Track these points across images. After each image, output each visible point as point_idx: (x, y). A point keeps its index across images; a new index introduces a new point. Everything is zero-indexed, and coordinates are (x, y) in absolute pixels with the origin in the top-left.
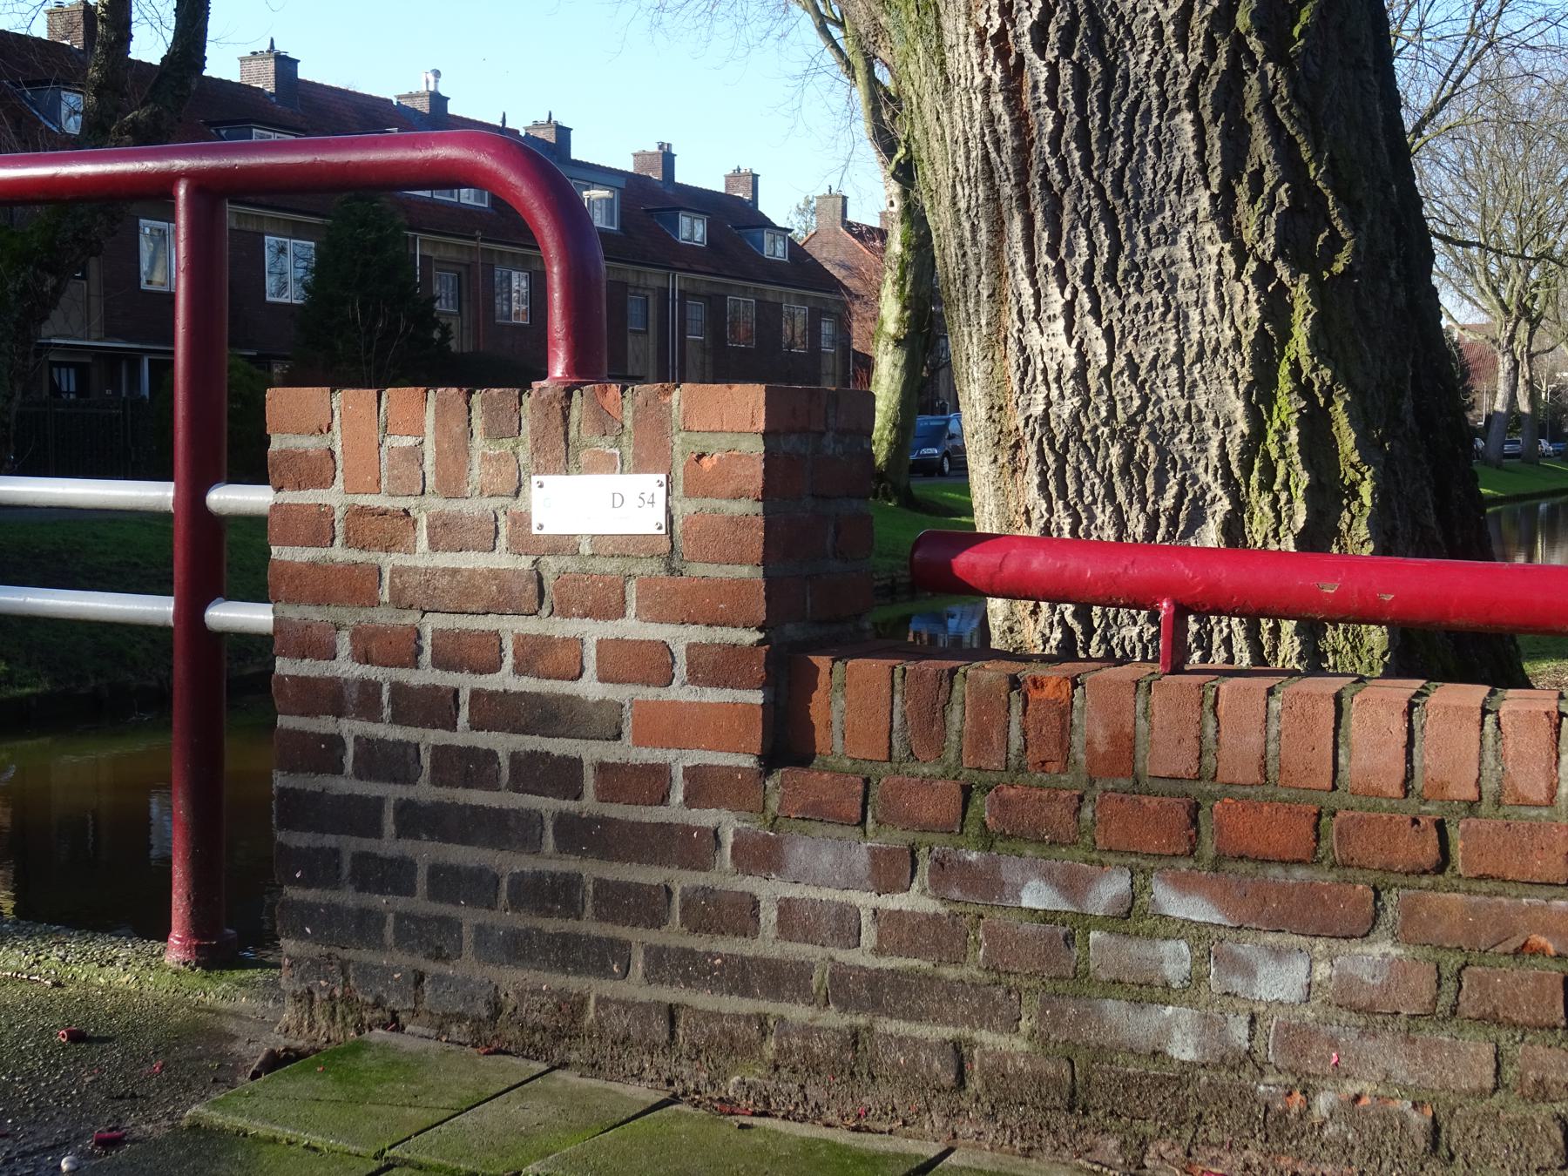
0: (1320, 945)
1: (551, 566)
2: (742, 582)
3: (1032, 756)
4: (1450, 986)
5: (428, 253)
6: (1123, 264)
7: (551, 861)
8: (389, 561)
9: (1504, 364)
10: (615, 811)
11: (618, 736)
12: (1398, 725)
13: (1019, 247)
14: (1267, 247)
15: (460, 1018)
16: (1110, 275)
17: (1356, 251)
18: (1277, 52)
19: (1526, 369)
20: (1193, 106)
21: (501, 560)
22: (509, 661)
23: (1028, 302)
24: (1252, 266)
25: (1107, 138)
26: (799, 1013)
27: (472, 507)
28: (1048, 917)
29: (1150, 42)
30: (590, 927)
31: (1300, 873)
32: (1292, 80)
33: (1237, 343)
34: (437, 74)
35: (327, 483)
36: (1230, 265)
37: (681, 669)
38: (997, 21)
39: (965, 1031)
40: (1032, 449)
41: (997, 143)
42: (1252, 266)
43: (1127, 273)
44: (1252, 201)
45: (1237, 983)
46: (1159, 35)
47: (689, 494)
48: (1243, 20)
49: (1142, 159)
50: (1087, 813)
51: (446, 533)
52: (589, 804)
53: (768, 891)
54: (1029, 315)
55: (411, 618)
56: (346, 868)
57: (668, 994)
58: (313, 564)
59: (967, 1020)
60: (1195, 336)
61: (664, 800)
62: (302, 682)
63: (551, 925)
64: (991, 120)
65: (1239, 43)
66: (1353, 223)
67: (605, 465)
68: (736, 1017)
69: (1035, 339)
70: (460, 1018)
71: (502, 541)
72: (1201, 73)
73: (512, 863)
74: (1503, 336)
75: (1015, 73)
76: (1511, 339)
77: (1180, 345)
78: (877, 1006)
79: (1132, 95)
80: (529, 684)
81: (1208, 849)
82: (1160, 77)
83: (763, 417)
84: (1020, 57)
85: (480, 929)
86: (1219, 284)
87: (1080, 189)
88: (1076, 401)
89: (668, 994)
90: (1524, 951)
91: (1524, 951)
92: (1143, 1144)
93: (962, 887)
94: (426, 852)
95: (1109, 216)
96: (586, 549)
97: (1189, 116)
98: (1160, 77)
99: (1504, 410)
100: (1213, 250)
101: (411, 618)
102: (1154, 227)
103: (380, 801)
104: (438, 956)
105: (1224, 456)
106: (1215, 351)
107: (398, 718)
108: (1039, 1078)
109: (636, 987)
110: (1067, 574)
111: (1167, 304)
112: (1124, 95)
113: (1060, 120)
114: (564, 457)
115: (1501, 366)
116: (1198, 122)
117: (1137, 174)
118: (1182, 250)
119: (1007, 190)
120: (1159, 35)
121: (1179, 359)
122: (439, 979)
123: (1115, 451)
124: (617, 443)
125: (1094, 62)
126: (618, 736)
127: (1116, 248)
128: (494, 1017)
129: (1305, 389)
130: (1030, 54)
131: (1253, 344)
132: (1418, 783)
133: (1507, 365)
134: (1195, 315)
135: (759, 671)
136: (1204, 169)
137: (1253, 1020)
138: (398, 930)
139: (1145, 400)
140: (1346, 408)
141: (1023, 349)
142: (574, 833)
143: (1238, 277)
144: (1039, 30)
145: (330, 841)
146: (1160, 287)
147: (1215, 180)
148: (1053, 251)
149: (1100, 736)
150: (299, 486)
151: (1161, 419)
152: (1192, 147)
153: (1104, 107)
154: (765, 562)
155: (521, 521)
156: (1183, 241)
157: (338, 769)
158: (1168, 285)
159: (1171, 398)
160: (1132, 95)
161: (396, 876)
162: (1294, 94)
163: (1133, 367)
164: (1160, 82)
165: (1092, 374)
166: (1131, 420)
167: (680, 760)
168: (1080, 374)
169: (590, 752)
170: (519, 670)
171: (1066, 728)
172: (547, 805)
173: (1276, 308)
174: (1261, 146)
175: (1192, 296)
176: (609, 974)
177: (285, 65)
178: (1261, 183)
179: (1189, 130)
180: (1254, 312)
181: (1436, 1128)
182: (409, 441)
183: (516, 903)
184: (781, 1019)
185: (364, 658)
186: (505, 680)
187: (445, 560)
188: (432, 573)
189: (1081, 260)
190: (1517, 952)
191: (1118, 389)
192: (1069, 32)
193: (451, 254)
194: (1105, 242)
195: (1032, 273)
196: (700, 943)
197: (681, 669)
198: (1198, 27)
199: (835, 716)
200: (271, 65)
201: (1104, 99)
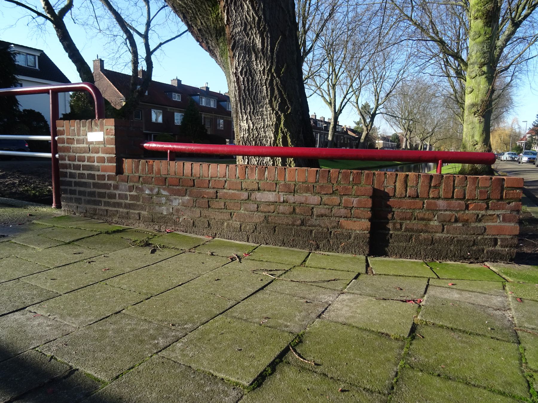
0: (180, 197)
1: (91, 146)
2: (112, 148)
3: (149, 172)
4: (195, 203)
5: (205, 116)
6: (255, 111)
7: (93, 189)
8: (72, 146)
9: (405, 140)
10: (99, 182)
11: (99, 171)
12: (190, 166)
13: (239, 109)
14: (277, 109)
15: (82, 212)
16: (253, 113)
17: (291, 110)
18: (278, 76)
20: (266, 85)
21: (85, 145)
22: (86, 160)
23: (241, 118)
24: (275, 112)
25: (252, 90)
26: (121, 210)
27: (81, 137)
28: (149, 195)
29: (259, 74)
30: (97, 199)
31: (178, 187)
32: (281, 81)
33: (272, 125)
34: (207, 83)
35: (64, 134)
36: (271, 112)
37: (106, 161)
38: (235, 70)
39: (140, 211)
40: (241, 142)
41: (236, 91)
42: (275, 112)
43: (256, 113)
44: (275, 101)
45: (171, 203)
46: (260, 73)
47: (106, 135)
48: (273, 71)
49: (258, 94)
50: (153, 180)
51: (79, 141)
52: (96, 181)
53: (117, 192)
54: (241, 120)
55: (75, 154)
56: (68, 192)
57: (106, 208)
58: (63, 147)
59: (140, 210)
60: (266, 124)
61: (105, 180)
62: (62, 164)
63: (93, 199)
64: (235, 87)
65: (272, 75)
66: (291, 106)
67: (96, 131)
68: (114, 211)
69: (242, 124)
70: (82, 212)
71: (85, 143)
72: (267, 80)
73: (88, 190)
74: (405, 134)
75: (238, 79)
76: (406, 135)
77: (264, 125)
78: (130, 208)
79: (256, 83)
80: (89, 163)
81: (167, 184)
82: (261, 80)
84: (239, 77)
85: (84, 200)
86: (270, 115)
87: (248, 99)
88: (248, 134)
89: (106, 208)
90: (203, 197)
91: (203, 197)
92: (161, 226)
93: (139, 191)
94: (78, 189)
95: (253, 103)
96: (95, 143)
97: (265, 87)
98: (261, 80)
100: (269, 109)
101: (75, 154)
102: (260, 105)
103: (72, 181)
104: (80, 204)
105: (270, 143)
106: (269, 126)
107: (74, 169)
108: (148, 218)
109: (103, 207)
111: (262, 118)
112: (255, 83)
113: (245, 87)
114: (91, 130)
116: (266, 87)
117: (257, 96)
118: (264, 109)
119: (238, 99)
120: (260, 73)
121: (264, 127)
122: (80, 207)
123: (254, 142)
124: (98, 128)
125: (250, 77)
126: (99, 171)
127: (254, 109)
128: (86, 212)
129: (283, 132)
130: (240, 76)
131: (275, 125)
132: (193, 174)
134: (266, 120)
135: (115, 160)
136: (267, 95)
137: (173, 208)
138: (75, 200)
139: (258, 134)
140: (289, 135)
141: (240, 126)
142: (95, 185)
143: (273, 114)
144: (241, 72)
145: (66, 187)
146: (261, 115)
147: (269, 98)
148: (244, 109)
149: (156, 169)
150: (61, 135)
151: (261, 137)
152: (265, 92)
153: (252, 85)
154: (116, 145)
155: (87, 139)
156: (264, 108)
157: (67, 177)
158: (262, 115)
159: (262, 134)
160: (256, 83)
161: (119, 205)
162: (281, 83)
163: (256, 128)
164: (261, 81)
165: (250, 130)
166: (256, 137)
167: (107, 174)
168: (249, 130)
169: (97, 173)
170: (88, 161)
171: (153, 168)
172: (91, 181)
173: (278, 119)
174: (276, 92)
175: (266, 117)
176: (99, 205)
177: (179, 81)
178: (276, 98)
179: (265, 89)
180: (275, 120)
181: (194, 222)
182: (73, 128)
183: (88, 196)
184: (119, 211)
185: (69, 160)
186: (86, 163)
187: (78, 145)
188: (77, 147)
189: (249, 111)
190: (202, 198)
191: (254, 132)
192: (246, 72)
193: (209, 116)
194: (252, 108)
195: (241, 113)
196: (109, 200)
197: (106, 161)
198: (266, 72)
199: (126, 167)
200: (177, 81)
201: (252, 84)
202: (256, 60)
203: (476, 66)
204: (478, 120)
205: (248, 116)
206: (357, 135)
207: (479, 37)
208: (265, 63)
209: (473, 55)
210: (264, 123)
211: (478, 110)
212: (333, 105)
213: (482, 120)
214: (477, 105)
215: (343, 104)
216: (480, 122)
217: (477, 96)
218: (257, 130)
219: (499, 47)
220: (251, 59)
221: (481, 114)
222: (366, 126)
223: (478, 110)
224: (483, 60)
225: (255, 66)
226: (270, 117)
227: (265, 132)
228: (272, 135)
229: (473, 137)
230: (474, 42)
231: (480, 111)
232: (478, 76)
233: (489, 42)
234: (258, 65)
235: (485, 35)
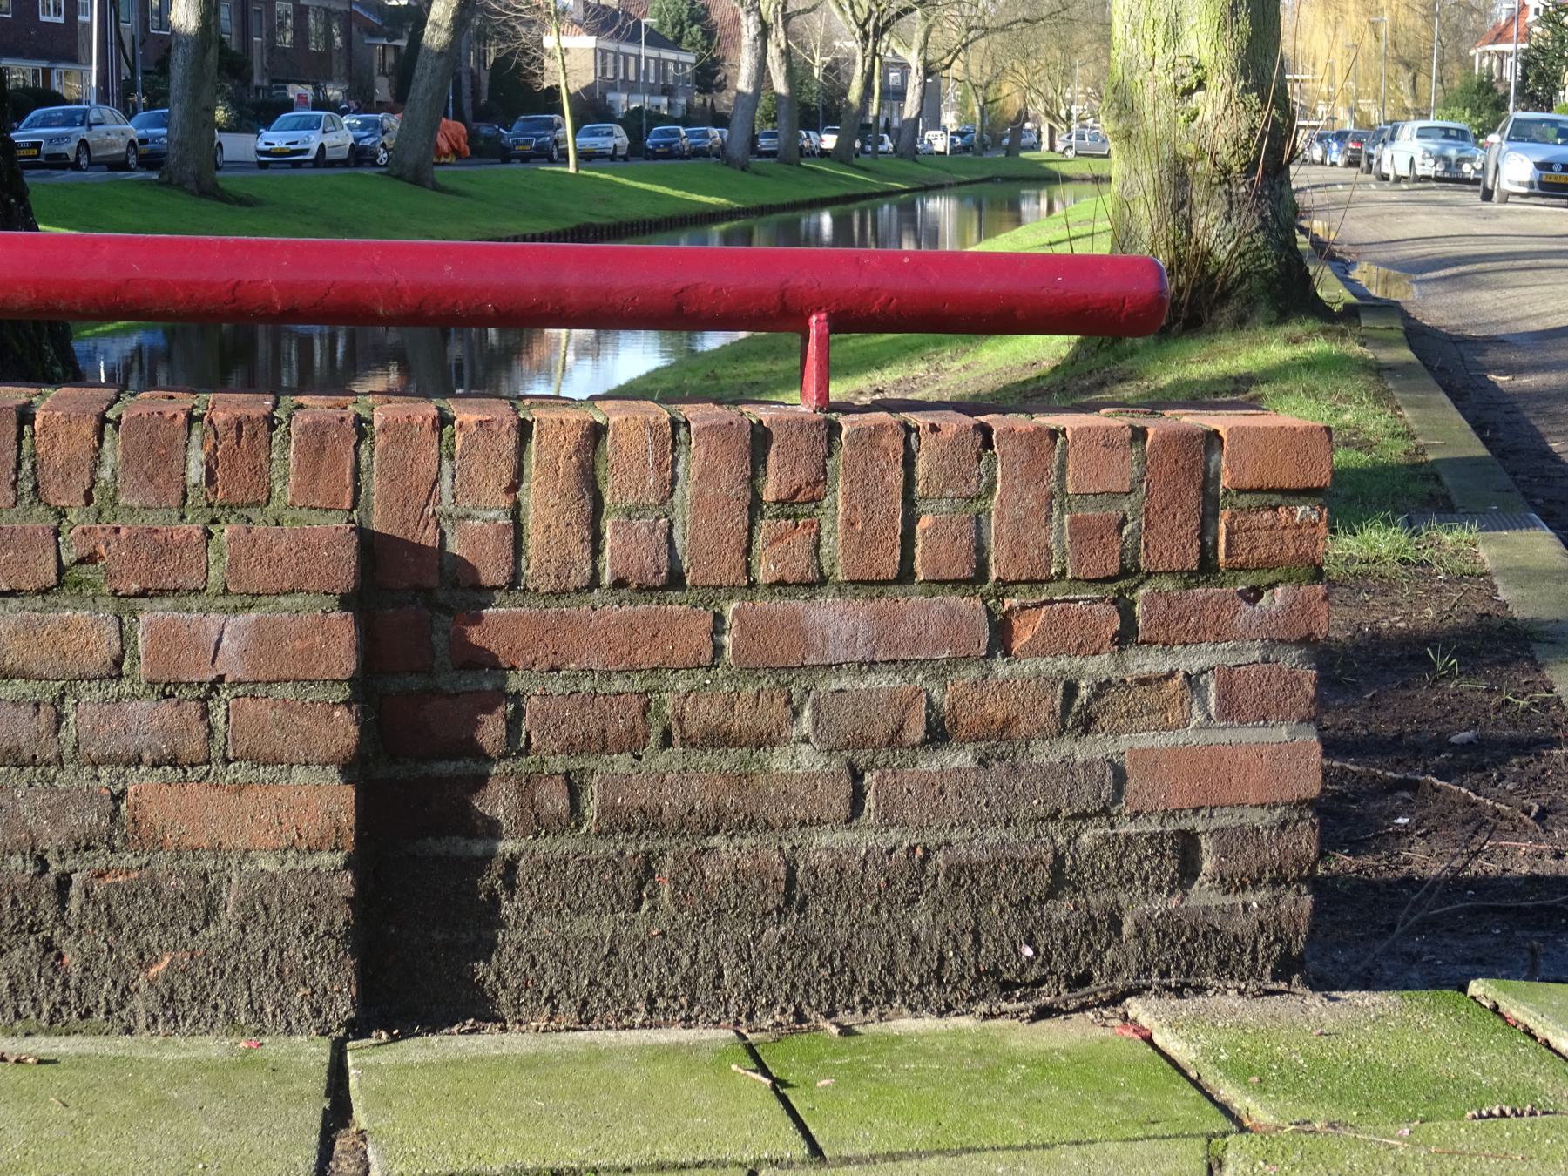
9: (749, 27)
19: (781, 34)
83: (351, 1082)
99: (750, 90)
110: (504, 374)
115: (744, 30)
133: (752, 29)
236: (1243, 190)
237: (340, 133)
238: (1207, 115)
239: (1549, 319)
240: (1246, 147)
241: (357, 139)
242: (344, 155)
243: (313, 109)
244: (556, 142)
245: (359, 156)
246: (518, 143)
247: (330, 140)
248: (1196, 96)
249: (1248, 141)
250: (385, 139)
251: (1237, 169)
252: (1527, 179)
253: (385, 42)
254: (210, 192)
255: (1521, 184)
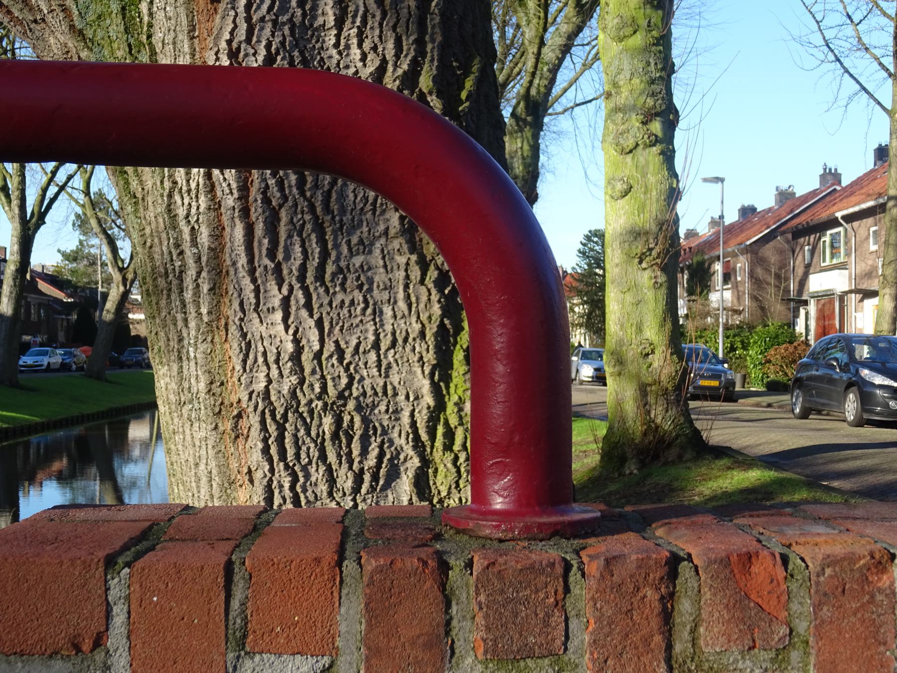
16: (320, 277)
33: (422, 334)
43: (334, 275)
60: (388, 328)
69: (255, 327)
77: (377, 335)
86: (406, 286)
87: (296, 205)
88: (294, 379)
100: (402, 260)
102: (355, 240)
106: (406, 340)
111: (366, 301)
118: (376, 258)
121: (376, 345)
127: (325, 255)
131: (436, 335)
134: (388, 311)
139: (351, 378)
143: (422, 282)
146: (360, 287)
151: (364, 394)
156: (377, 252)
158: (366, 286)
159: (371, 378)
165: (307, 358)
166: (341, 396)
168: (296, 357)
180: (436, 310)
189: (296, 263)
194: (315, 250)
195: (252, 272)
202: (340, 24)
203: (634, 117)
204: (651, 278)
205: (291, 289)
206: (69, 296)
207: (635, 32)
208: (391, 45)
209: (621, 83)
210: (379, 325)
211: (650, 250)
212: (15, 195)
213: (662, 278)
214: (647, 233)
215: (51, 192)
216: (656, 286)
217: (642, 208)
218: (341, 359)
219: (547, 64)
220: (314, 18)
221: (659, 261)
222: (121, 270)
223: (650, 250)
224: (650, 102)
225: (334, 52)
226: (408, 297)
227: (385, 370)
228: (425, 386)
229: (640, 329)
230: (621, 46)
231: (654, 253)
232: (641, 146)
233: (660, 52)
234: (347, 47)
235: (650, 31)
236: (673, 398)
237: (57, 357)
238: (656, 365)
239: (773, 445)
240: (674, 379)
241: (63, 360)
242: (58, 367)
243: (40, 347)
244: (144, 360)
245: (64, 367)
246: (127, 360)
247: (52, 360)
248: (650, 356)
249: (675, 376)
250: (75, 359)
251: (670, 388)
252: (591, 375)
253: (64, 317)
254: (15, 385)
255: (589, 377)
